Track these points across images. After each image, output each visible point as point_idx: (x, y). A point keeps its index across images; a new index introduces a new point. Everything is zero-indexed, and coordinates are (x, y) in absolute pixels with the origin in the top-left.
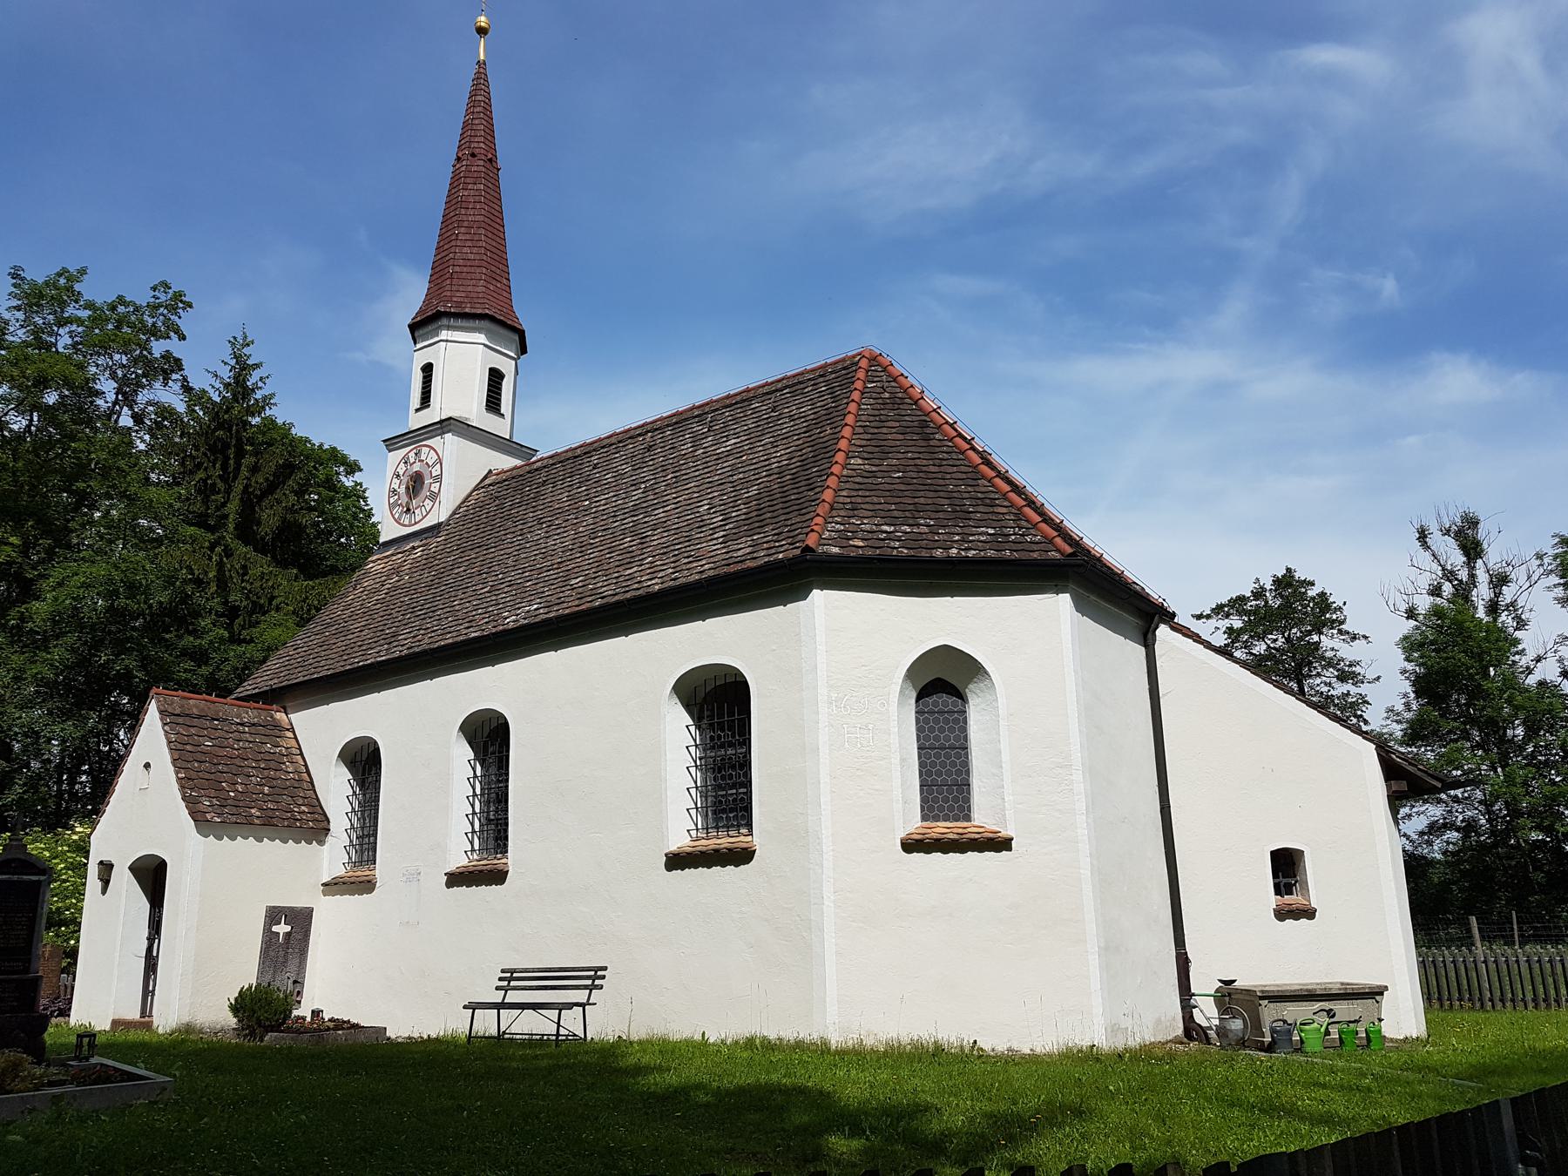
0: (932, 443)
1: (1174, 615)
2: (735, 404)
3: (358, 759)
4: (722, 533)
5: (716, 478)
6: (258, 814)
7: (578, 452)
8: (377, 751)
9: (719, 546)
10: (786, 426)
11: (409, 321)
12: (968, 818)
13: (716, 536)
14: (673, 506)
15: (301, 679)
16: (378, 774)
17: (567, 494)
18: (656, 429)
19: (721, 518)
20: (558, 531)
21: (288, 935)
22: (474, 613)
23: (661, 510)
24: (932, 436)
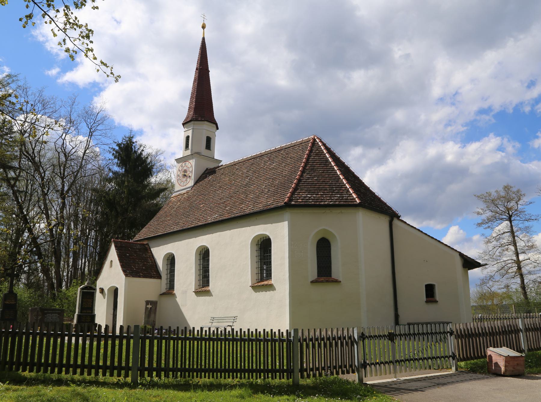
0: (328, 167)
1: (400, 217)
2: (277, 151)
3: (169, 259)
4: (267, 195)
5: (269, 176)
6: (142, 275)
7: (233, 164)
8: (174, 256)
9: (265, 200)
10: (289, 161)
11: (182, 122)
12: (331, 276)
13: (265, 196)
14: (256, 185)
15: (153, 236)
16: (117, 309)
17: (228, 178)
18: (255, 158)
19: (267, 190)
20: (225, 191)
21: (150, 308)
22: (200, 217)
23: (253, 186)
24: (328, 165)
